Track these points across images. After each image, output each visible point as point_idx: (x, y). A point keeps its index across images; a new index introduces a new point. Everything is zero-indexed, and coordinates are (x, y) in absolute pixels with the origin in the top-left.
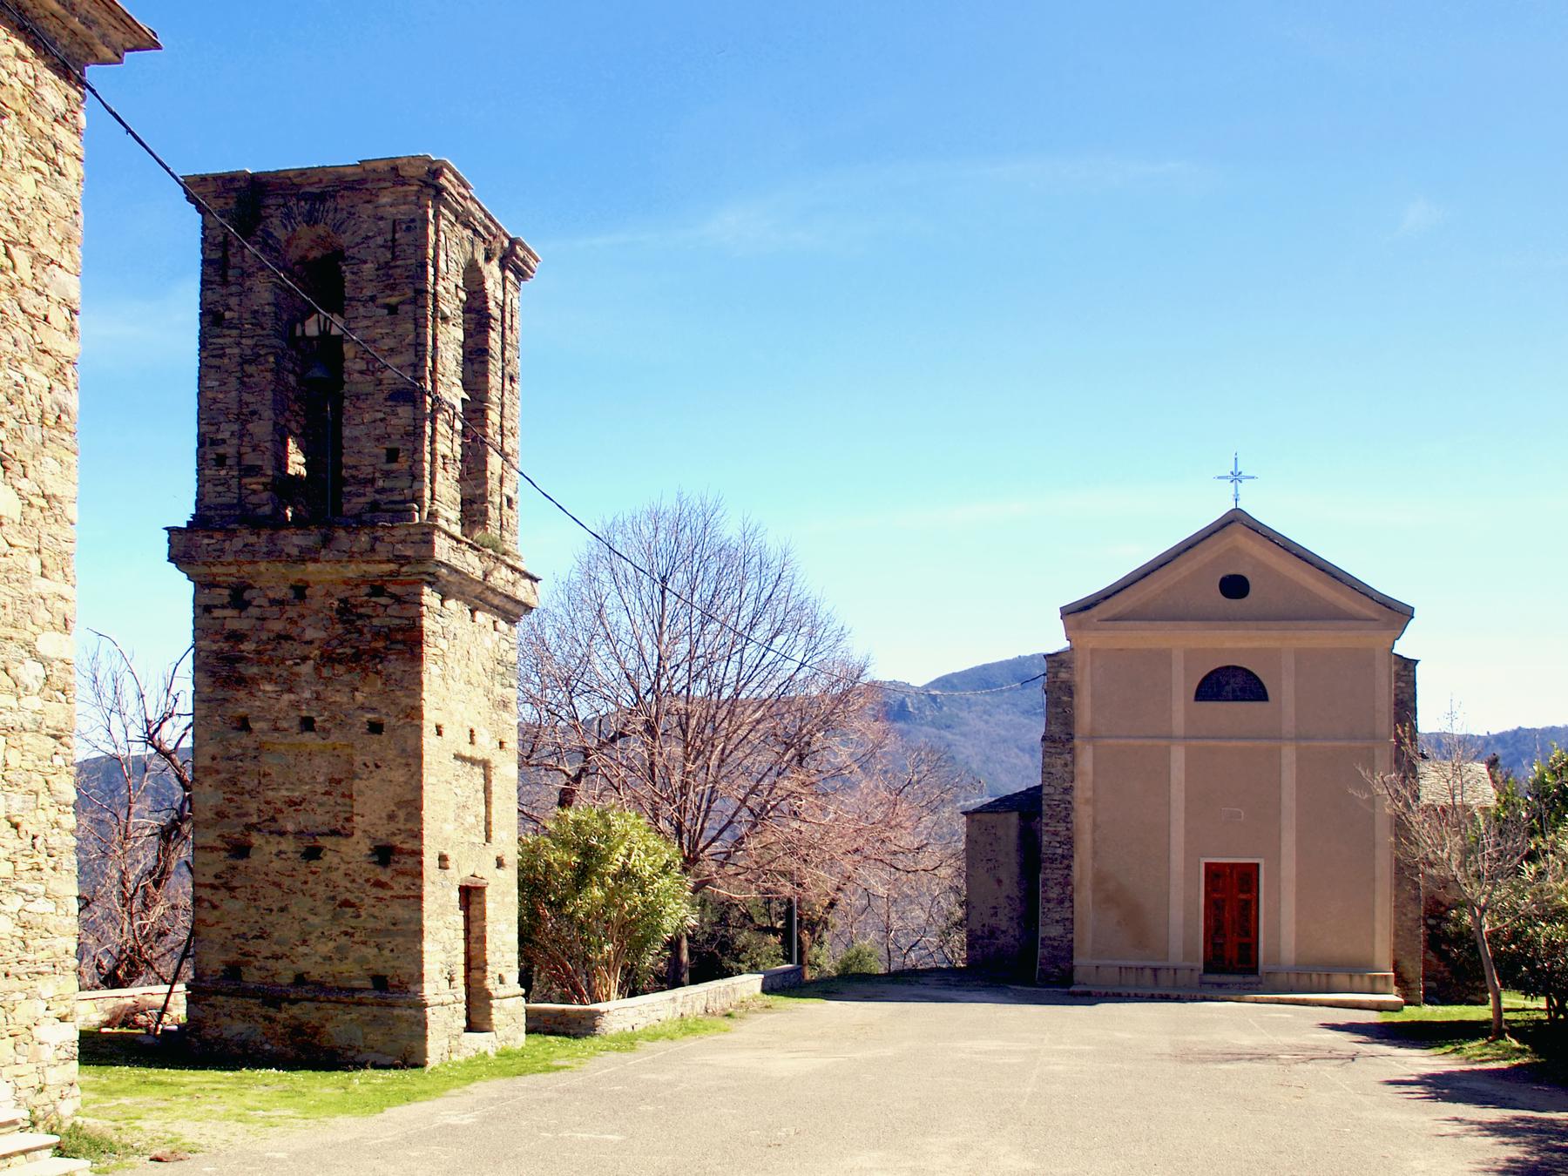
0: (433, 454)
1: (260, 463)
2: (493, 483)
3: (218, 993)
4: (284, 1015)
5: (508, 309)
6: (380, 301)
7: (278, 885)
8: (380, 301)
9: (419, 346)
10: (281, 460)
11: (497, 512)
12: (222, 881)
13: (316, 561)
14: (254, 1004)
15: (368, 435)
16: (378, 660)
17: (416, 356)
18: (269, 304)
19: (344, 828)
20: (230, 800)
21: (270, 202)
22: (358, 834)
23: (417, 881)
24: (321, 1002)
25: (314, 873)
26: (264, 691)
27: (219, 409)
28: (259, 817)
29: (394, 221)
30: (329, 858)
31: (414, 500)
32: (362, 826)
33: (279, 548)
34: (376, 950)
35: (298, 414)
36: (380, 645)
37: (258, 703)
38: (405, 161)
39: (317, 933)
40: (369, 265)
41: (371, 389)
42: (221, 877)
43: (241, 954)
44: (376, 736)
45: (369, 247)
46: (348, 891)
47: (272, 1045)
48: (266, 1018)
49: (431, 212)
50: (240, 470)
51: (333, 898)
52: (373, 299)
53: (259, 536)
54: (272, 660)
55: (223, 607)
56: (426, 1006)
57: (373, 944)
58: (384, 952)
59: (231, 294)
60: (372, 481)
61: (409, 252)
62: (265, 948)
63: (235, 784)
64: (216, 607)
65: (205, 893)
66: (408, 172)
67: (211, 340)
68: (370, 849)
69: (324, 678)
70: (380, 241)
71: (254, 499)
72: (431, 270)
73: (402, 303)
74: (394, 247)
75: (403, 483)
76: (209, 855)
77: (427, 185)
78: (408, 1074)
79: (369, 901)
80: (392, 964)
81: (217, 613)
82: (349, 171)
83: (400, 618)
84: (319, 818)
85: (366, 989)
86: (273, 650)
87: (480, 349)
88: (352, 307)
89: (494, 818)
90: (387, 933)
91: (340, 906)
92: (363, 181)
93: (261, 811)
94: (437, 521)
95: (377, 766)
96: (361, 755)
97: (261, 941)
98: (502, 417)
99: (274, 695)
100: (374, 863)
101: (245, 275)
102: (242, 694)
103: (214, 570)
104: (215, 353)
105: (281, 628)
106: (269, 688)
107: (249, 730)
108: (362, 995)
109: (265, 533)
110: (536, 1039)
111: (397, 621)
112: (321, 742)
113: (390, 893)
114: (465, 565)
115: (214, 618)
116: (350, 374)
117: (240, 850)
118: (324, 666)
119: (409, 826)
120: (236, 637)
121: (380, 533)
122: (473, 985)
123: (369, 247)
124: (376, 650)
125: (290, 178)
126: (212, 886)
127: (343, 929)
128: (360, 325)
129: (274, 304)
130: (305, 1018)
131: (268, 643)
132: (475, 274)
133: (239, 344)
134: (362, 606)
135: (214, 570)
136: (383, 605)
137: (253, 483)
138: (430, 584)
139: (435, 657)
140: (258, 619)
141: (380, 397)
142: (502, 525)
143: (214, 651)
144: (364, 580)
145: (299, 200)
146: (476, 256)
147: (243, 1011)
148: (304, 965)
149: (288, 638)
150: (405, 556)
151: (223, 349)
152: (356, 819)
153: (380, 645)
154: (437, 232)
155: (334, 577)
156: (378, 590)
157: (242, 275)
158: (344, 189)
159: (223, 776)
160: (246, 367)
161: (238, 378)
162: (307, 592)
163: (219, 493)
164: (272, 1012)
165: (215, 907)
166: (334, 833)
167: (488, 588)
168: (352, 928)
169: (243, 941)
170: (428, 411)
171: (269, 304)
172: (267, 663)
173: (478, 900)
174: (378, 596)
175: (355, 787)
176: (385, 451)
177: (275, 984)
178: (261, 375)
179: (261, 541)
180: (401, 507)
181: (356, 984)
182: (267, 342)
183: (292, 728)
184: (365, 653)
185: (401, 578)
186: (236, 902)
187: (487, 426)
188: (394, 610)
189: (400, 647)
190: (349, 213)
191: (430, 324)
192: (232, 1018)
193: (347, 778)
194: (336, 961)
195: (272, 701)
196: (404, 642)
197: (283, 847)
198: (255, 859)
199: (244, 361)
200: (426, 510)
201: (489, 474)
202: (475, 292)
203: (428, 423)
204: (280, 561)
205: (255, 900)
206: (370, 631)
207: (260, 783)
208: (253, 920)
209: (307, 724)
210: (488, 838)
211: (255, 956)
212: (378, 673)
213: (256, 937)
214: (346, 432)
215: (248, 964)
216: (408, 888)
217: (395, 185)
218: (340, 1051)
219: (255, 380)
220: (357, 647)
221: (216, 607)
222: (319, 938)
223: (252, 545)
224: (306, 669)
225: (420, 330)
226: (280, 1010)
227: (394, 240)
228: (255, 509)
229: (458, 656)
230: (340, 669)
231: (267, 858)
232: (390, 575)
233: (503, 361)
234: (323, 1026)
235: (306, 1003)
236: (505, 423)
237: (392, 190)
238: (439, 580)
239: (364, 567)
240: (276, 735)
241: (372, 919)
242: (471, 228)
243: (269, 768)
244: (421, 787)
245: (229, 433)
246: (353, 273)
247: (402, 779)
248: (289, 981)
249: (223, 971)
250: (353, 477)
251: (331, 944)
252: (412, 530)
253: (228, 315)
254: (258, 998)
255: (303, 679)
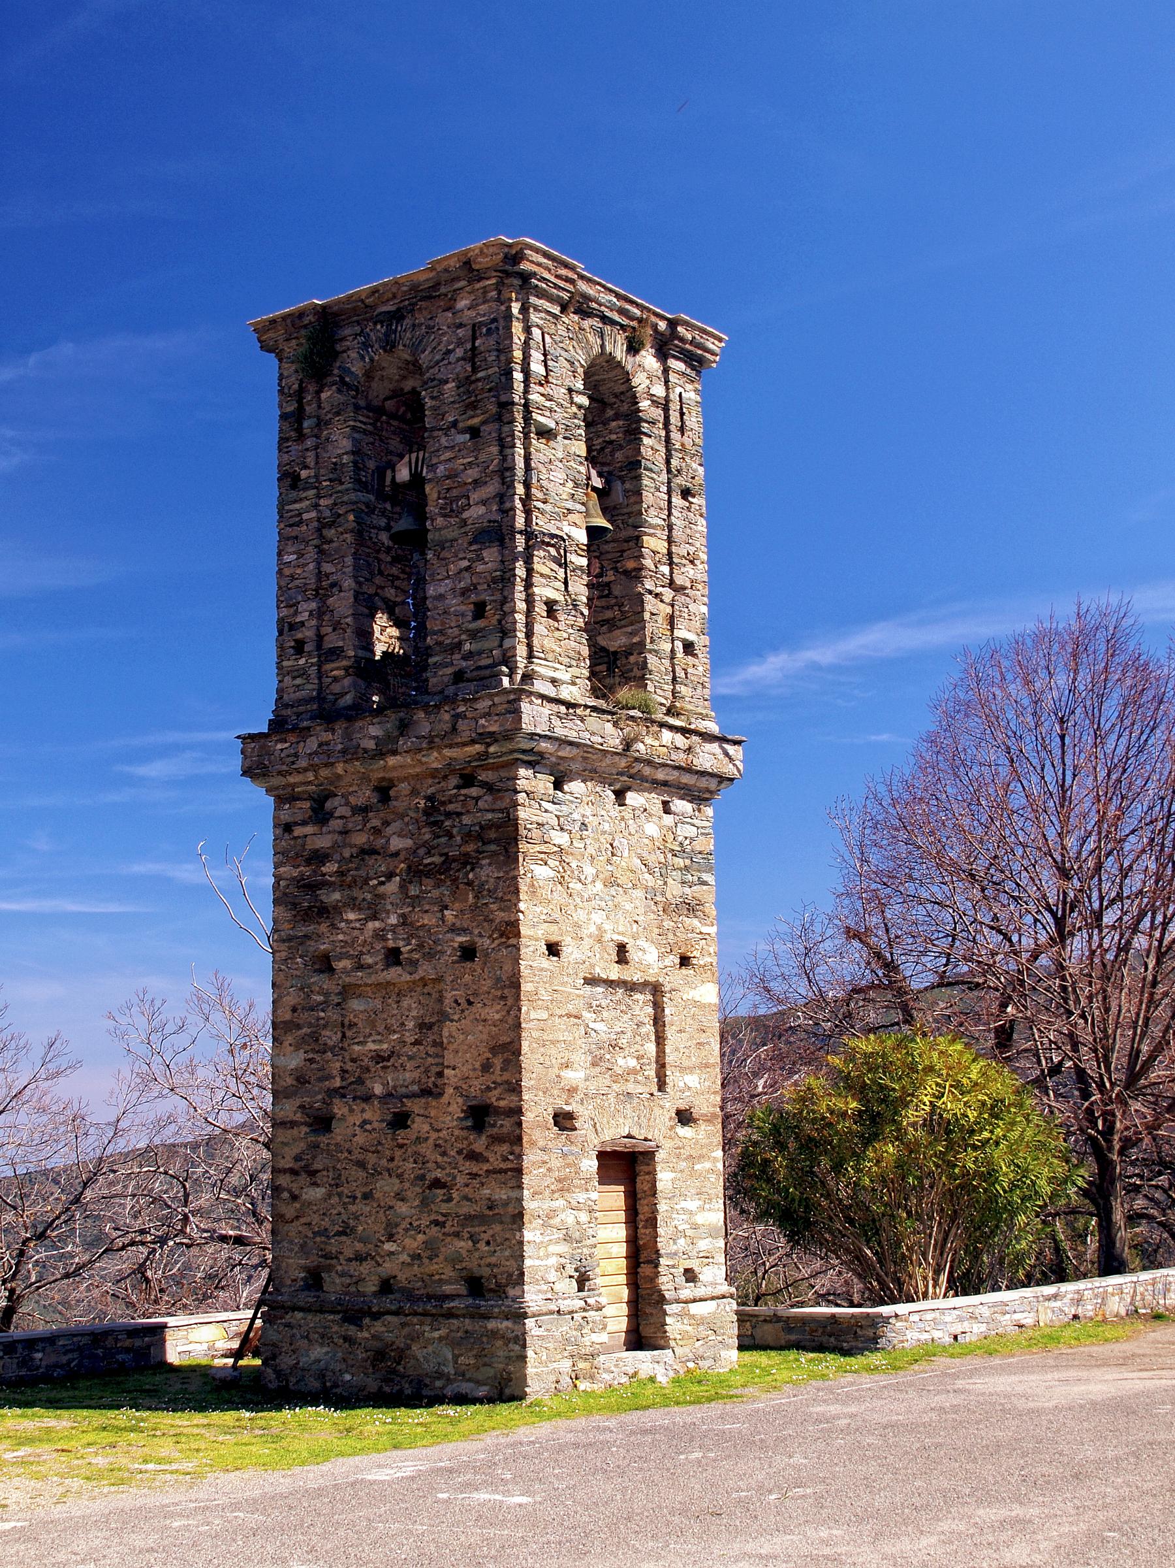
0: (530, 600)
1: (341, 644)
2: (655, 625)
3: (295, 1308)
4: (366, 1334)
5: (674, 407)
6: (461, 425)
7: (361, 1164)
8: (461, 425)
9: (505, 471)
10: (365, 638)
11: (667, 662)
12: (303, 1163)
13: (395, 753)
14: (333, 1321)
15: (453, 590)
16: (469, 868)
17: (503, 484)
18: (346, 453)
19: (436, 1086)
20: (311, 1061)
21: (347, 331)
22: (450, 1091)
23: (516, 1149)
24: (407, 1315)
25: (401, 1146)
26: (348, 922)
27: (298, 587)
28: (343, 1079)
29: (474, 325)
30: (419, 1126)
31: (505, 662)
32: (453, 1080)
33: (354, 742)
34: (470, 1243)
35: (398, 578)
36: (470, 848)
37: (341, 937)
38: (477, 251)
39: (405, 1224)
40: (452, 385)
41: (455, 534)
42: (301, 1159)
43: (322, 1256)
44: (469, 964)
45: (450, 363)
46: (439, 1167)
47: (353, 1375)
48: (346, 1339)
49: (515, 308)
50: (319, 656)
51: (422, 1178)
52: (454, 424)
53: (333, 731)
54: (355, 881)
55: (304, 823)
56: (525, 1316)
57: (466, 1235)
58: (478, 1245)
59: (307, 450)
60: (459, 645)
61: (490, 359)
62: (350, 1247)
63: (317, 1040)
64: (296, 824)
65: (284, 1180)
66: (482, 262)
67: (287, 508)
68: (463, 1111)
69: (412, 897)
70: (459, 353)
71: (336, 688)
72: (518, 376)
73: (484, 423)
74: (474, 356)
75: (492, 642)
76: (289, 1132)
77: (508, 274)
78: (503, 1409)
79: (461, 1180)
80: (488, 1260)
81: (298, 831)
82: (422, 278)
83: (493, 811)
84: (407, 1076)
85: (459, 1296)
86: (357, 869)
87: (631, 463)
88: (434, 438)
89: (670, 1058)
90: (481, 1219)
91: (430, 1188)
92: (437, 285)
93: (347, 1071)
94: (533, 684)
95: (470, 1003)
96: (452, 990)
97: (344, 1238)
98: (670, 541)
99: (358, 925)
100: (467, 1128)
101: (321, 423)
102: (323, 928)
103: (291, 779)
104: (292, 521)
105: (364, 840)
106: (351, 916)
107: (331, 970)
108: (452, 1304)
109: (340, 727)
110: (750, 1357)
111: (489, 816)
112: (408, 978)
113: (486, 1167)
114: (587, 735)
115: (295, 838)
116: (432, 520)
117: (322, 1123)
118: (410, 882)
119: (506, 1076)
120: (318, 858)
121: (462, 709)
122: (643, 1285)
123: (450, 363)
124: (466, 854)
125: (362, 301)
126: (294, 1172)
127: (433, 1217)
128: (442, 458)
129: (353, 453)
130: (389, 1337)
131: (351, 862)
132: (618, 371)
133: (316, 506)
134: (451, 802)
135: (291, 779)
136: (474, 798)
137: (335, 669)
138: (530, 764)
139: (542, 856)
140: (341, 833)
141: (463, 542)
142: (674, 679)
143: (294, 878)
144: (450, 769)
145: (375, 324)
146: (609, 348)
147: (321, 1330)
148: (389, 1267)
149: (373, 852)
150: (489, 733)
151: (300, 514)
152: (446, 1071)
153: (470, 848)
154: (527, 330)
155: (418, 770)
156: (468, 780)
157: (318, 425)
158: (420, 300)
159: (305, 1030)
160: (325, 532)
161: (316, 547)
162: (392, 793)
163: (298, 686)
164: (352, 1330)
165: (294, 1198)
166: (426, 1092)
167: (637, 760)
168: (444, 1215)
169: (323, 1239)
170: (520, 549)
171: (346, 453)
172: (350, 887)
173: (644, 1168)
174: (469, 787)
175: (445, 1033)
176: (472, 606)
177: (360, 1294)
178: (342, 539)
179: (335, 738)
180: (487, 672)
181: (448, 1289)
182: (345, 498)
183: (376, 964)
184: (454, 861)
185: (491, 761)
186: (318, 1190)
187: (642, 556)
188: (486, 801)
189: (493, 847)
190: (428, 327)
191: (518, 443)
192: (309, 1340)
193: (438, 1021)
194: (426, 1261)
195: (356, 933)
196: (496, 841)
197: (367, 1116)
198: (339, 1132)
199: (322, 525)
200: (520, 672)
201: (647, 616)
202: (622, 393)
203: (520, 564)
204: (357, 759)
205: (337, 1185)
206: (459, 833)
207: (344, 1036)
208: (335, 1212)
209: (393, 957)
210: (662, 1085)
211: (337, 1258)
212: (469, 884)
213: (339, 1234)
214: (431, 591)
215: (329, 1269)
216: (505, 1159)
217: (470, 282)
218: (427, 1381)
219: (334, 545)
220: (446, 854)
221: (296, 824)
222: (407, 1230)
223: (327, 743)
224: (392, 887)
225: (508, 451)
226: (361, 1328)
227: (474, 348)
228: (336, 700)
229: (591, 850)
230: (428, 883)
231: (349, 1131)
232: (479, 760)
233: (669, 471)
234: (409, 1347)
235: (389, 1318)
236: (674, 549)
237: (467, 289)
238: (543, 758)
239: (447, 752)
240: (359, 974)
241: (465, 1203)
242: (597, 316)
243: (355, 1016)
244: (518, 1026)
245: (307, 614)
246: (432, 398)
247: (497, 1017)
248: (374, 1289)
249: (302, 1279)
250: (439, 643)
251: (421, 1237)
252: (497, 700)
253: (304, 474)
254: (338, 1312)
255: (388, 901)
